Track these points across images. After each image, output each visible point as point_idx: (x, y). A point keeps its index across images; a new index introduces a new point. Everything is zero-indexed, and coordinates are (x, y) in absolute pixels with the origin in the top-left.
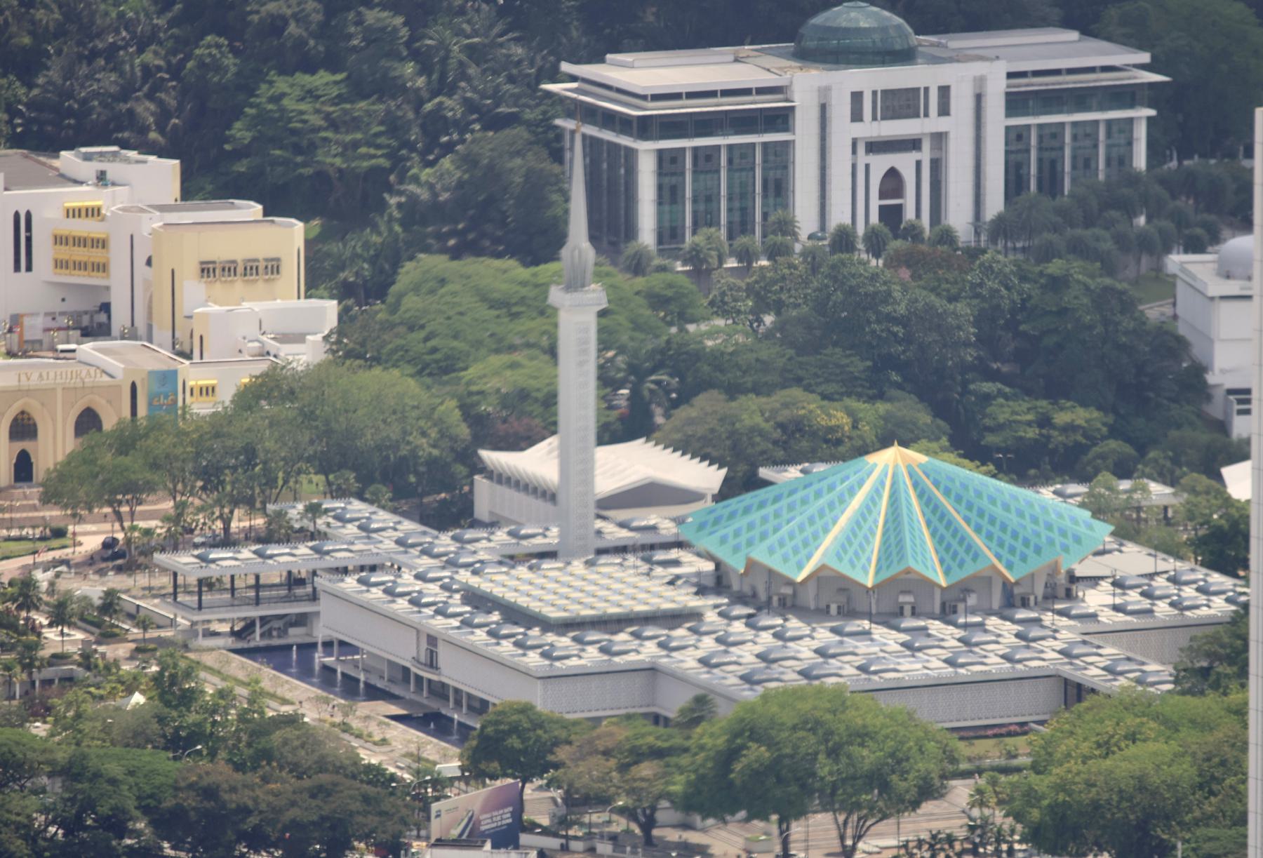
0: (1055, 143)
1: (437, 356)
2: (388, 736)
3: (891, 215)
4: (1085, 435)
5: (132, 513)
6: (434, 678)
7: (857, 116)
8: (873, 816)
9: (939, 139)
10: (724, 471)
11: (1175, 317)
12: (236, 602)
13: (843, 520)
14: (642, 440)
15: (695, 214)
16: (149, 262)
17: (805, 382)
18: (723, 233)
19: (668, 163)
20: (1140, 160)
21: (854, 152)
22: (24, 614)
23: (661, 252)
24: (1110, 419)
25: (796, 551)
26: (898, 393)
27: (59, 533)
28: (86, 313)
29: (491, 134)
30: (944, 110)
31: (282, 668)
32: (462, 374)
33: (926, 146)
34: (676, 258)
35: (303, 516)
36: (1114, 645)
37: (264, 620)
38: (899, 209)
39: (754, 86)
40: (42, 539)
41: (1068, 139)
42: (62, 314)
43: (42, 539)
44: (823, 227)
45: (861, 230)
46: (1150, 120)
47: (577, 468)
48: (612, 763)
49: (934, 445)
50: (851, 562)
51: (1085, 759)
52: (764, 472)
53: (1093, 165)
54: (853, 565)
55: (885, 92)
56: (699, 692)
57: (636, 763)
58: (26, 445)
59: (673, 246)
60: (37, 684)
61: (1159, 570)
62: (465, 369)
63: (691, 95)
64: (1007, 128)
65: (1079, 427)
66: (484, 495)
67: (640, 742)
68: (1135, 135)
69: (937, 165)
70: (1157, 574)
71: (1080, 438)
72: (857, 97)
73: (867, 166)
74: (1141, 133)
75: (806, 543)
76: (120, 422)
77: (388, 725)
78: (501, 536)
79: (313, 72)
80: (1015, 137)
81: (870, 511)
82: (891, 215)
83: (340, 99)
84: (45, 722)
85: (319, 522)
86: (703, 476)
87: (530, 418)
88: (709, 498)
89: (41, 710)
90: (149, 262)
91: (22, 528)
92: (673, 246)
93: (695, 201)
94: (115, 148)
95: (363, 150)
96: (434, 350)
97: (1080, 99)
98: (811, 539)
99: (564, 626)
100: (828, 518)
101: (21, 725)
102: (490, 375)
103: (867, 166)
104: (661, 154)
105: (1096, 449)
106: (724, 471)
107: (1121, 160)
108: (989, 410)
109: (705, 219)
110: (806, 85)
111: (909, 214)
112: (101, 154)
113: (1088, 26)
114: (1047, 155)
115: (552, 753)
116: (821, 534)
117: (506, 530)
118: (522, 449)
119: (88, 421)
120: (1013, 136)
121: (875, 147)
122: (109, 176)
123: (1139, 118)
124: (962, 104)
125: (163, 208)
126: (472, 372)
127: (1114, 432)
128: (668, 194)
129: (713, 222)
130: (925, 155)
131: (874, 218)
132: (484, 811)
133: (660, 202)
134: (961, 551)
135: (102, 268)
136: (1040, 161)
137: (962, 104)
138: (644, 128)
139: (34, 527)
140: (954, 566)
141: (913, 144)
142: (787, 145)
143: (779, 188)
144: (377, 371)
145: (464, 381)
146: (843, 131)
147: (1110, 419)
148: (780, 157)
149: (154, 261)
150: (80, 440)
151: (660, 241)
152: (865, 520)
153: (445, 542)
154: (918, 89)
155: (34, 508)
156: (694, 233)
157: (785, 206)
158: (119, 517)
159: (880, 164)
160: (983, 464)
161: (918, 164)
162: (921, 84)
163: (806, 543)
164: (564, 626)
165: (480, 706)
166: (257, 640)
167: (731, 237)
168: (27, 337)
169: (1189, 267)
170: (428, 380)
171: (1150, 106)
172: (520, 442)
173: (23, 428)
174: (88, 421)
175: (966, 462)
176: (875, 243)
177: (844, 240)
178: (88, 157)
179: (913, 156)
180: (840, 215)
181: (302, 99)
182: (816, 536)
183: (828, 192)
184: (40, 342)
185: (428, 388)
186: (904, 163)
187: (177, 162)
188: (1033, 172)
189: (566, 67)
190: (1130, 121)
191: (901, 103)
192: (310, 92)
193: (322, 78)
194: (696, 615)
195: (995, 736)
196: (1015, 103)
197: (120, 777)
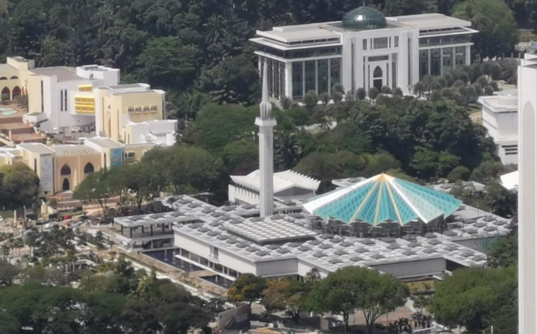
0: (437, 56)
1: (215, 141)
2: (201, 285)
3: (378, 84)
4: (450, 164)
5: (105, 200)
6: (217, 263)
7: (365, 48)
8: (378, 313)
9: (395, 56)
10: (319, 182)
11: (482, 119)
12: (144, 235)
13: (364, 201)
14: (289, 170)
15: (306, 84)
16: (109, 107)
17: (348, 148)
18: (316, 92)
19: (296, 67)
20: (468, 62)
21: (364, 60)
22: (68, 240)
23: (294, 99)
24: (459, 158)
25: (347, 213)
26: (383, 151)
27: (80, 209)
28: (87, 125)
29: (231, 57)
30: (397, 45)
31: (162, 259)
32: (224, 147)
33: (390, 58)
34: (300, 101)
35: (168, 202)
36: (465, 245)
37: (154, 241)
38: (381, 81)
39: (327, 38)
40: (74, 211)
41: (442, 54)
42: (78, 126)
43: (74, 211)
44: (353, 88)
45: (367, 90)
46: (471, 46)
47: (269, 183)
48: (283, 295)
49: (396, 171)
50: (367, 217)
51: (457, 292)
52: (334, 182)
53: (451, 63)
54: (368, 218)
55: (375, 39)
56: (314, 267)
57: (292, 295)
58: (66, 176)
59: (299, 97)
60: (74, 267)
61: (480, 216)
62: (224, 145)
63: (304, 42)
64: (420, 51)
65: (448, 162)
66: (233, 193)
67: (294, 287)
68: (466, 52)
69: (394, 65)
70: (479, 218)
71: (448, 166)
72: (365, 41)
73: (369, 66)
74: (468, 51)
75: (351, 210)
76: (101, 169)
77: (201, 281)
78: (239, 208)
79: (167, 36)
80: (423, 55)
81: (374, 198)
82: (378, 84)
83: (176, 46)
84: (77, 281)
85: (174, 204)
86: (313, 184)
87: (249, 163)
88: (314, 192)
89: (75, 277)
90: (109, 107)
91: (66, 207)
92: (299, 97)
93: (306, 80)
94: (96, 65)
95: (185, 64)
96: (214, 138)
97: (447, 39)
98: (352, 209)
99: (263, 243)
100: (358, 201)
101: (69, 283)
102: (233, 148)
103: (369, 66)
104: (294, 64)
105: (454, 170)
106: (319, 182)
107: (461, 61)
108: (415, 156)
109: (310, 86)
110: (345, 37)
111: (384, 84)
112: (91, 68)
113: (445, 9)
114: (434, 60)
115: (261, 292)
116: (356, 206)
117: (241, 206)
118: (246, 175)
119: (89, 168)
120: (422, 53)
121: (371, 59)
122: (94, 77)
123: (468, 46)
124: (403, 43)
125: (114, 87)
126: (228, 146)
127: (461, 163)
128: (296, 79)
129: (313, 88)
130: (390, 61)
131: (372, 86)
132: (237, 315)
133: (294, 80)
134: (408, 213)
135: (93, 109)
136: (432, 62)
137: (403, 43)
138: (286, 54)
139: (70, 207)
140: (405, 218)
141: (386, 58)
142: (340, 59)
143: (337, 75)
144: (192, 148)
145: (224, 150)
146: (360, 54)
147: (459, 158)
148: (337, 63)
149: (111, 107)
150: (87, 175)
151: (294, 95)
152: (372, 201)
153: (219, 210)
154: (387, 38)
155: (71, 200)
156: (306, 92)
157: (339, 81)
158: (101, 202)
159: (374, 65)
160: (414, 177)
161: (388, 65)
162: (388, 36)
163: (351, 210)
164: (263, 243)
165: (233, 273)
166: (152, 249)
167: (319, 93)
168: (66, 135)
169: (486, 101)
170: (211, 150)
171: (471, 42)
172: (246, 172)
173: (66, 170)
174: (89, 168)
175: (407, 176)
176: (373, 95)
177: (361, 94)
178: (87, 69)
179: (386, 62)
180: (359, 85)
181: (163, 46)
182: (354, 208)
183: (355, 76)
184: (70, 137)
185: (212, 153)
186: (382, 64)
187: (118, 70)
188: (429, 65)
189: (258, 32)
190: (464, 47)
191: (381, 42)
192: (166, 43)
193: (170, 38)
194: (311, 238)
195: (422, 280)
196: (422, 42)
197: (106, 305)
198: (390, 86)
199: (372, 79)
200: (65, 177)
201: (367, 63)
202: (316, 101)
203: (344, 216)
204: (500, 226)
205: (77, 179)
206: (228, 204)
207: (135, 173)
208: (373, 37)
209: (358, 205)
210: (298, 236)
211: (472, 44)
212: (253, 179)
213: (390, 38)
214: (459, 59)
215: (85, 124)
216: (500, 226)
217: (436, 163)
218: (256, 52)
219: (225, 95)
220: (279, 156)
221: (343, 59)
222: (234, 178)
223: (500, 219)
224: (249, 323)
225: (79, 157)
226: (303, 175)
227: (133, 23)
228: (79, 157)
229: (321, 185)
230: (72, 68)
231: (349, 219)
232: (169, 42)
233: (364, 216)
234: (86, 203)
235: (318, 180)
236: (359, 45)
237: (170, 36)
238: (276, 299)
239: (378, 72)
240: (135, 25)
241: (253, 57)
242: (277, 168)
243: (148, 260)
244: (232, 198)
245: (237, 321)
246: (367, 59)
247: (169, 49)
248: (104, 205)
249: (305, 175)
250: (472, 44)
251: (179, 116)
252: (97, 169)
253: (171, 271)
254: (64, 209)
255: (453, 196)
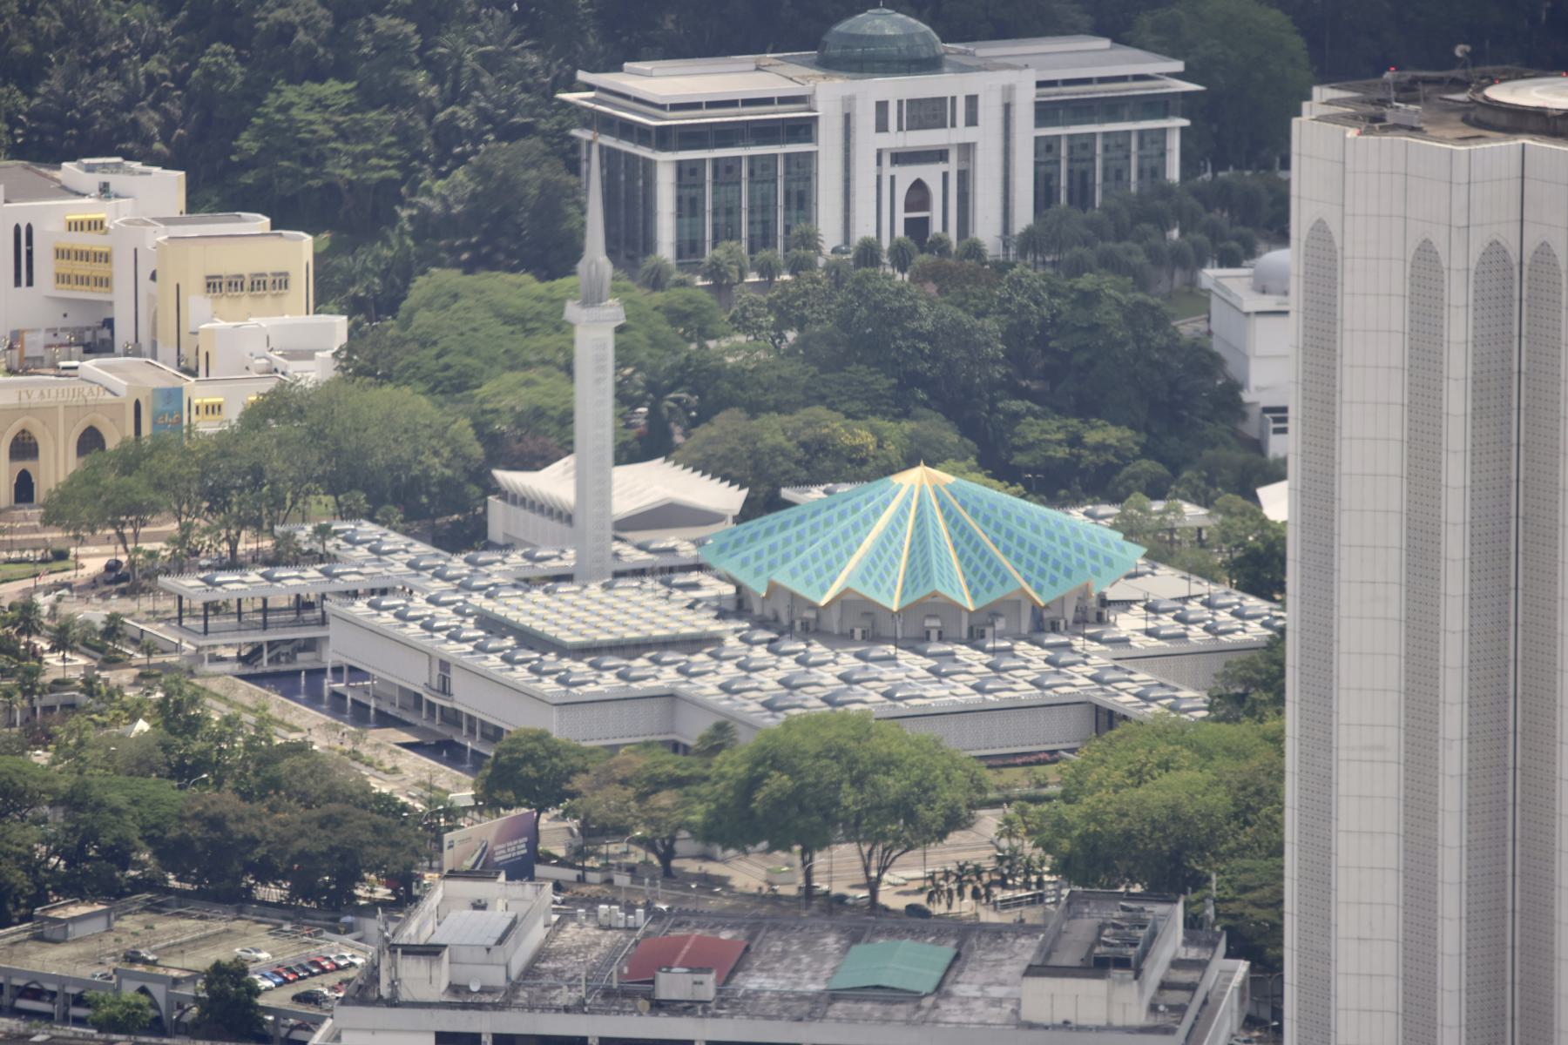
0: (1086, 154)
1: (450, 373)
3: (917, 228)
4: (1117, 455)
5: (136, 535)
7: (882, 127)
9: (967, 149)
10: (745, 492)
11: (1210, 333)
14: (661, 460)
16: (153, 277)
19: (687, 175)
20: (1173, 172)
21: (879, 163)
22: (24, 639)
23: (679, 265)
24: (1143, 438)
25: (819, 573)
26: (925, 411)
27: (61, 556)
28: (88, 329)
29: (505, 144)
30: (972, 120)
31: (290, 694)
33: (953, 156)
36: (1147, 670)
37: (272, 645)
39: (776, 95)
40: (44, 561)
42: (64, 330)
43: (44, 561)
45: (886, 244)
47: (593, 488)
48: (630, 792)
49: (962, 465)
50: (876, 584)
51: (1117, 788)
52: (787, 493)
53: (1125, 177)
55: (910, 102)
56: (721, 719)
57: (655, 792)
58: (27, 464)
62: (479, 386)
64: (1037, 139)
66: (499, 516)
67: (659, 770)
69: (964, 178)
70: (1191, 597)
72: (882, 107)
73: (893, 178)
74: (1174, 144)
75: (829, 566)
78: (516, 558)
80: (1045, 148)
81: (895, 532)
82: (917, 228)
83: (350, 109)
84: (46, 750)
85: (329, 544)
86: (725, 497)
87: (545, 436)
88: (730, 520)
89: (42, 738)
90: (153, 277)
93: (715, 213)
94: (118, 160)
95: (374, 161)
96: (447, 367)
97: (1112, 108)
99: (579, 652)
100: (852, 540)
101: (22, 753)
102: (505, 393)
103: (893, 178)
104: (680, 165)
106: (745, 492)
107: (1153, 171)
108: (1018, 429)
109: (725, 232)
110: (830, 94)
111: (936, 227)
112: (104, 165)
113: (1119, 32)
114: (1077, 166)
115: (569, 782)
118: (538, 469)
119: (90, 440)
120: (1043, 146)
121: (900, 158)
122: (112, 188)
123: (1173, 128)
124: (990, 113)
125: (167, 221)
126: (486, 389)
127: (1147, 452)
128: (688, 206)
129: (734, 235)
130: (952, 167)
131: (900, 232)
137: (990, 113)
138: (663, 138)
139: (35, 549)
140: (982, 589)
141: (940, 155)
142: (810, 156)
143: (802, 201)
145: (478, 399)
146: (868, 141)
148: (803, 168)
150: (82, 460)
152: (890, 542)
153: (458, 564)
154: (945, 99)
155: (35, 530)
156: (714, 246)
157: (808, 219)
158: (122, 539)
159: (907, 175)
160: (1012, 484)
161: (945, 175)
163: (829, 566)
164: (579, 652)
166: (264, 665)
167: (752, 250)
170: (441, 398)
171: (1183, 116)
172: (535, 461)
173: (24, 447)
174: (90, 440)
175: (994, 482)
177: (868, 254)
178: (90, 169)
179: (939, 168)
180: (864, 228)
181: (311, 109)
182: (839, 559)
183: (853, 205)
184: (41, 359)
185: (441, 406)
186: (931, 174)
188: (1062, 183)
189: (582, 76)
190: (1163, 131)
191: (928, 113)
192: (319, 101)
193: (332, 87)
194: (715, 640)
195: (1024, 764)
196: (1045, 113)
198: (953, 233)
199: (901, 215)
200: (20, 466)
201: (888, 170)
202: (742, 276)
203: (808, 582)
204: (1246, 622)
205: (57, 466)
206: (489, 546)
207: (224, 455)
208: (905, 96)
209: (850, 553)
210: (678, 634)
211: (1186, 123)
212: (554, 482)
213: (954, 99)
214: (1147, 164)
215: (86, 324)
216: (1246, 622)
217: (1075, 451)
218: (574, 132)
219: (484, 250)
220: (1024, 893)
221: (821, 156)
222: (505, 477)
223: (1252, 602)
224: (533, 870)
225: (61, 410)
226: (699, 473)
227: (226, 42)
228: (61, 410)
229: (748, 501)
230: (265, 390)
231: (824, 590)
232: (326, 98)
233: (865, 582)
234: (79, 540)
235: (741, 488)
236: (865, 119)
237: (331, 81)
238: (605, 801)
239: (918, 195)
240: (228, 48)
241: (567, 146)
242: (628, 453)
243: (250, 694)
244: (496, 532)
245: (497, 859)
246: (886, 160)
247: (327, 116)
248: (130, 546)
249: (703, 474)
250: (1186, 123)
251: (354, 308)
252: (112, 442)
253: (318, 726)
254: (15, 555)
255: (1119, 536)
